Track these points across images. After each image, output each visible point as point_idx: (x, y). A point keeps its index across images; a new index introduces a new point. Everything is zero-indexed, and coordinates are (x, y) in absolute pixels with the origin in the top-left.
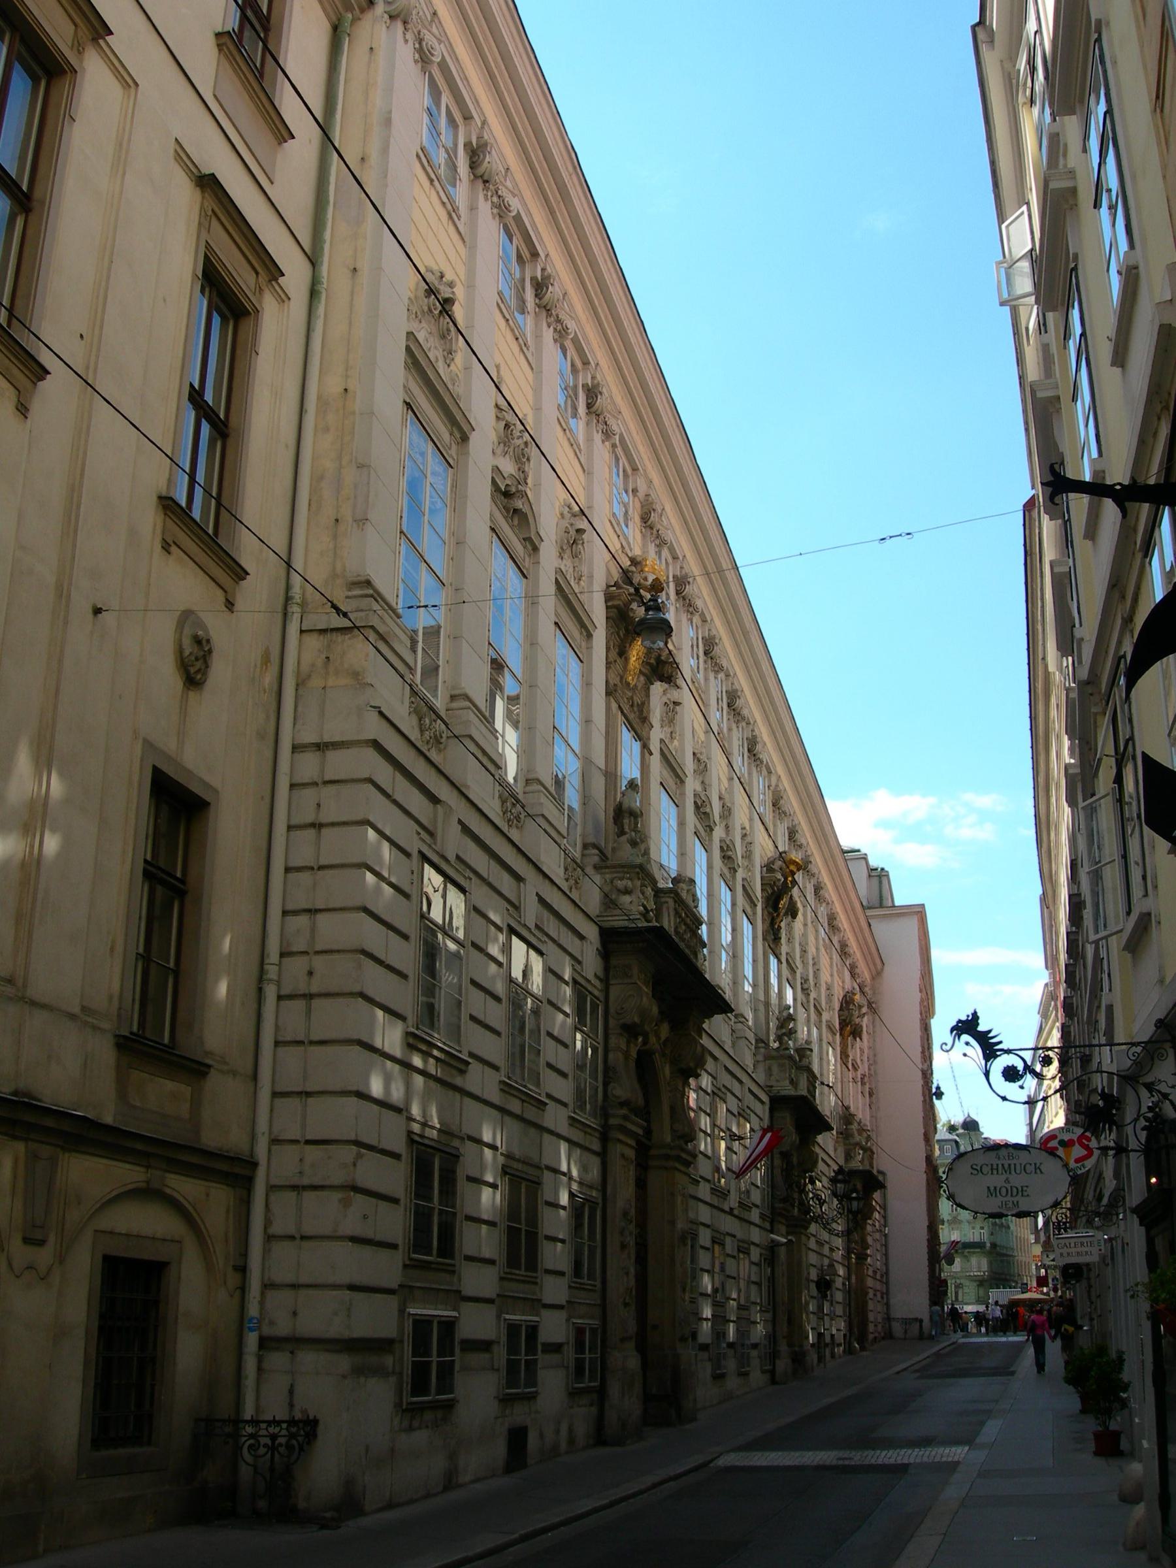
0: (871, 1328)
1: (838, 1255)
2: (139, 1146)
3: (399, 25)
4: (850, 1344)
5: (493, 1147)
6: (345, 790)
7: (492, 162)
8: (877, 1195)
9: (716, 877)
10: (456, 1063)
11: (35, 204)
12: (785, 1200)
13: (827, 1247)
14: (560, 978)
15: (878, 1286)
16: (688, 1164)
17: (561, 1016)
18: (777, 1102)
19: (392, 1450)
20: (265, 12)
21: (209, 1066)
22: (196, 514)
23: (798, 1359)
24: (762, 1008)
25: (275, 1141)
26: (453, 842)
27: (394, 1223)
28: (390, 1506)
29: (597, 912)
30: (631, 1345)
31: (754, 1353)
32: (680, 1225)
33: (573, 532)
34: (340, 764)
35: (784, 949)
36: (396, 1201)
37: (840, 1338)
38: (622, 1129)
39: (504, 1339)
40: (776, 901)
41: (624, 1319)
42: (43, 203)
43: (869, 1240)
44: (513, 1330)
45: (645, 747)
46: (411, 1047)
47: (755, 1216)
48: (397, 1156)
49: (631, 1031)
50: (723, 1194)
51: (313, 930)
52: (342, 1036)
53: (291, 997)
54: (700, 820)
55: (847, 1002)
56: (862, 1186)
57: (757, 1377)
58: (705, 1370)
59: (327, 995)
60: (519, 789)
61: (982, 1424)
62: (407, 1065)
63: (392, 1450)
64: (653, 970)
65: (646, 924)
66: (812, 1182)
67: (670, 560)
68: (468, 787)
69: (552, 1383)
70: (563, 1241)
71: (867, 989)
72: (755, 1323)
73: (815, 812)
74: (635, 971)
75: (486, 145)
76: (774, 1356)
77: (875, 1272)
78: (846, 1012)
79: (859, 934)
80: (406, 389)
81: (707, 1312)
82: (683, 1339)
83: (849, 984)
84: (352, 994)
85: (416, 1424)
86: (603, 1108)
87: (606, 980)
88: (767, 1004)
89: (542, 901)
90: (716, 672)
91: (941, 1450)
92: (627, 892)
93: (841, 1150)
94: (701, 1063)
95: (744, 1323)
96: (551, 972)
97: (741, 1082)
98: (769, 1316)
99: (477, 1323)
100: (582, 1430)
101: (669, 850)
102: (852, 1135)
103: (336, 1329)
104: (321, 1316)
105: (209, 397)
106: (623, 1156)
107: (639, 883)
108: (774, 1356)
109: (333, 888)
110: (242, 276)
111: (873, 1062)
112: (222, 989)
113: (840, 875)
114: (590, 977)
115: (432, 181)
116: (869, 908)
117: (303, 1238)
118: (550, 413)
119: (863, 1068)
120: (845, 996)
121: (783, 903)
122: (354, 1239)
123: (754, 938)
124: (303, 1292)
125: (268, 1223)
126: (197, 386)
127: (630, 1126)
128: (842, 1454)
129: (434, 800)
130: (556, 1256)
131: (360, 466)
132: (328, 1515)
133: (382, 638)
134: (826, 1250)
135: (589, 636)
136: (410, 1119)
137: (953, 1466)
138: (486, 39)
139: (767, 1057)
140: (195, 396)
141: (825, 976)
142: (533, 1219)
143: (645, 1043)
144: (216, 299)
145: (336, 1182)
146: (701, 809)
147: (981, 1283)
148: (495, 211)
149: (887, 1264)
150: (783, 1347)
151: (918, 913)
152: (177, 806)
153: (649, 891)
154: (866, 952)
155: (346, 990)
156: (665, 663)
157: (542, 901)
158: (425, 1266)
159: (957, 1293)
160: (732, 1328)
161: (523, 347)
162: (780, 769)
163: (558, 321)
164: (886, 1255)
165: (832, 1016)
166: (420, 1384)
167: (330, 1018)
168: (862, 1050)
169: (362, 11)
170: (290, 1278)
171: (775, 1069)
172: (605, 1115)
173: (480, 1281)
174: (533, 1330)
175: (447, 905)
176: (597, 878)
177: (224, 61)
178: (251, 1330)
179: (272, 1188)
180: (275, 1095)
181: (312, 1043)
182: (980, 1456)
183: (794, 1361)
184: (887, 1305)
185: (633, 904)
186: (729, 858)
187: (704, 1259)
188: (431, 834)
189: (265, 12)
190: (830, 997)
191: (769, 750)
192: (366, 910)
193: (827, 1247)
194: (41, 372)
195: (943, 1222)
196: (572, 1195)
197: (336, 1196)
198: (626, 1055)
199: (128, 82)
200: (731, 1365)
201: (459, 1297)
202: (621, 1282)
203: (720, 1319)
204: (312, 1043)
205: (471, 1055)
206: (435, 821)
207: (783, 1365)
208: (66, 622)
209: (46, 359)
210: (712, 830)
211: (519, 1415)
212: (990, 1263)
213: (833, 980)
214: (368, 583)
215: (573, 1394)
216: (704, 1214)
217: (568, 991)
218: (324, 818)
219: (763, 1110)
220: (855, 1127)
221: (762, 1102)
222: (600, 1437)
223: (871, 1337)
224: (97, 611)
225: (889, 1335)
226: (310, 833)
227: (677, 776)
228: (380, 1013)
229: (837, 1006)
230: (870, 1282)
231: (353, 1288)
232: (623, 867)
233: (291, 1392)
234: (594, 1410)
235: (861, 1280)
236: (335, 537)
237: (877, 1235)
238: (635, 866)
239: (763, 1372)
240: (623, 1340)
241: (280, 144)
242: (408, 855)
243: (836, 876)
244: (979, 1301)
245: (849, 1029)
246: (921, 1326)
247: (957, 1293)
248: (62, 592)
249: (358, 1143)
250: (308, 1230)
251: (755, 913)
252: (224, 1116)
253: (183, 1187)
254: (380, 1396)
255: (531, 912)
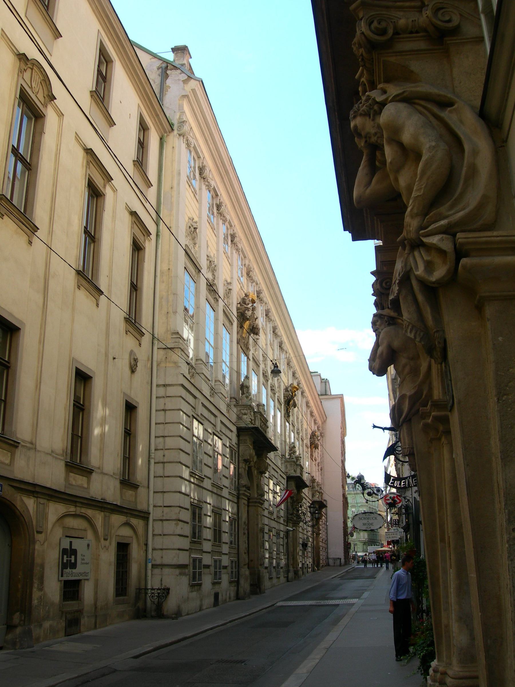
0: (321, 562)
1: (309, 534)
2: (125, 511)
3: (182, 138)
4: (313, 568)
5: (210, 504)
6: (173, 399)
7: (206, 172)
8: (324, 510)
9: (251, 369)
10: (201, 479)
11: (96, 240)
12: (292, 514)
13: (305, 530)
14: (226, 446)
15: (324, 545)
16: (262, 504)
17: (226, 459)
18: (289, 478)
19: (188, 598)
20: (104, 74)
21: (19, 443)
22: (15, 202)
23: (296, 573)
24: (283, 443)
25: (154, 506)
26: (201, 410)
27: (187, 530)
28: (188, 614)
29: (235, 421)
30: (246, 566)
31: (281, 570)
32: (260, 526)
33: (228, 290)
34: (171, 391)
35: (291, 418)
36: (188, 523)
37: (310, 565)
38: (244, 494)
39: (213, 565)
40: (289, 403)
41: (244, 557)
42: (99, 240)
43: (321, 527)
44: (215, 561)
45: (248, 358)
46: (191, 476)
47: (282, 521)
48: (188, 509)
49: (246, 461)
50: (271, 513)
51: (164, 443)
52: (174, 475)
53: (158, 463)
54: (264, 378)
55: (313, 435)
56: (319, 506)
57: (282, 579)
58: (267, 576)
59: (169, 462)
60: (193, 363)
61: (363, 593)
62: (190, 481)
63: (188, 598)
64: (254, 440)
65: (252, 426)
66: (301, 507)
67: (243, 258)
68: (202, 390)
69: (225, 578)
70: (227, 533)
71: (320, 428)
72: (282, 559)
73: (293, 339)
74: (248, 441)
75: (205, 166)
76: (288, 571)
77: (323, 540)
78: (313, 440)
79: (317, 407)
80: (185, 264)
81: (267, 556)
82: (261, 565)
83: (314, 428)
84: (177, 462)
85: (193, 590)
86: (238, 488)
87: (238, 444)
88: (285, 441)
89: (221, 422)
90: (252, 283)
91: (349, 600)
92: (245, 414)
93: (310, 493)
94: (266, 469)
95: (278, 559)
96: (224, 445)
97: (277, 472)
98: (286, 557)
99: (207, 560)
100: (233, 594)
101: (226, 353)
102: (315, 487)
103: (174, 562)
104: (170, 558)
105: (21, 151)
106: (244, 503)
107: (249, 411)
108: (288, 571)
109: (170, 430)
110: (99, 181)
111: (322, 457)
112: (140, 461)
113: (311, 386)
114: (234, 444)
115: (190, 186)
116: (322, 395)
117: (164, 535)
118: (205, 218)
119: (319, 460)
120: (312, 433)
121: (292, 402)
122: (179, 535)
123: (281, 417)
124: (164, 551)
125: (153, 530)
126: (16, 147)
127: (246, 493)
128: (317, 601)
129: (195, 397)
130: (225, 538)
131: (174, 294)
132: (173, 616)
133: (182, 350)
134: (305, 532)
135: (232, 324)
136: (191, 498)
137: (353, 604)
138: (205, 130)
139: (286, 461)
140: (15, 151)
141: (305, 426)
142: (220, 527)
143: (249, 464)
144: (25, 108)
145: (174, 518)
146: (211, 287)
147: (364, 543)
148: (207, 187)
149: (327, 537)
150: (291, 568)
151: (341, 397)
152: (130, 408)
153: (252, 413)
154: (320, 413)
155: (175, 461)
156: (255, 328)
157: (221, 422)
158: (194, 542)
159: (354, 548)
160: (274, 561)
161: (213, 229)
162: (290, 351)
163: (224, 216)
164: (327, 533)
165: (307, 441)
166: (194, 578)
167: (170, 469)
168: (318, 453)
169: (170, 132)
170: (160, 547)
171: (288, 466)
172: (239, 490)
173: (207, 546)
174: (200, 560)
175: (198, 430)
176: (235, 410)
177: (135, 169)
178: (149, 562)
179: (154, 520)
180: (154, 492)
181: (165, 477)
182: (362, 601)
183: (295, 573)
184: (327, 553)
185: (247, 418)
186: (273, 390)
187: (266, 537)
188: (215, 426)
189: (104, 74)
190: (306, 434)
191: (287, 345)
192: (181, 437)
193: (305, 530)
194: (36, 229)
195: (349, 518)
196: (230, 517)
197: (174, 522)
198: (245, 469)
199: (61, 115)
200: (274, 575)
201: (203, 552)
202: (243, 546)
203: (271, 558)
204: (165, 477)
205: (205, 476)
206: (195, 404)
207: (291, 575)
208: (108, 364)
209: (144, 331)
210: (268, 381)
211: (217, 588)
212: (369, 535)
213: (307, 427)
214: (178, 333)
215: (231, 582)
216: (266, 521)
217: (228, 450)
218: (167, 408)
219: (284, 482)
220: (315, 484)
221: (284, 479)
222: (238, 597)
223: (321, 565)
224: (114, 358)
225: (328, 565)
226: (163, 412)
227: (257, 365)
228: (184, 467)
229: (309, 437)
230: (321, 544)
231: (179, 549)
232: (243, 405)
233: (161, 580)
234: (236, 588)
235: (318, 543)
236: (167, 318)
237: (324, 526)
238: (248, 406)
239: (284, 577)
240: (244, 565)
241: (110, 127)
242: (189, 417)
243: (308, 382)
244: (363, 551)
245: (314, 445)
246: (340, 561)
247: (354, 548)
248: (106, 355)
249: (180, 507)
250: (165, 533)
251: (281, 408)
252: (144, 499)
253: (89, 512)
254: (185, 581)
255: (219, 426)
